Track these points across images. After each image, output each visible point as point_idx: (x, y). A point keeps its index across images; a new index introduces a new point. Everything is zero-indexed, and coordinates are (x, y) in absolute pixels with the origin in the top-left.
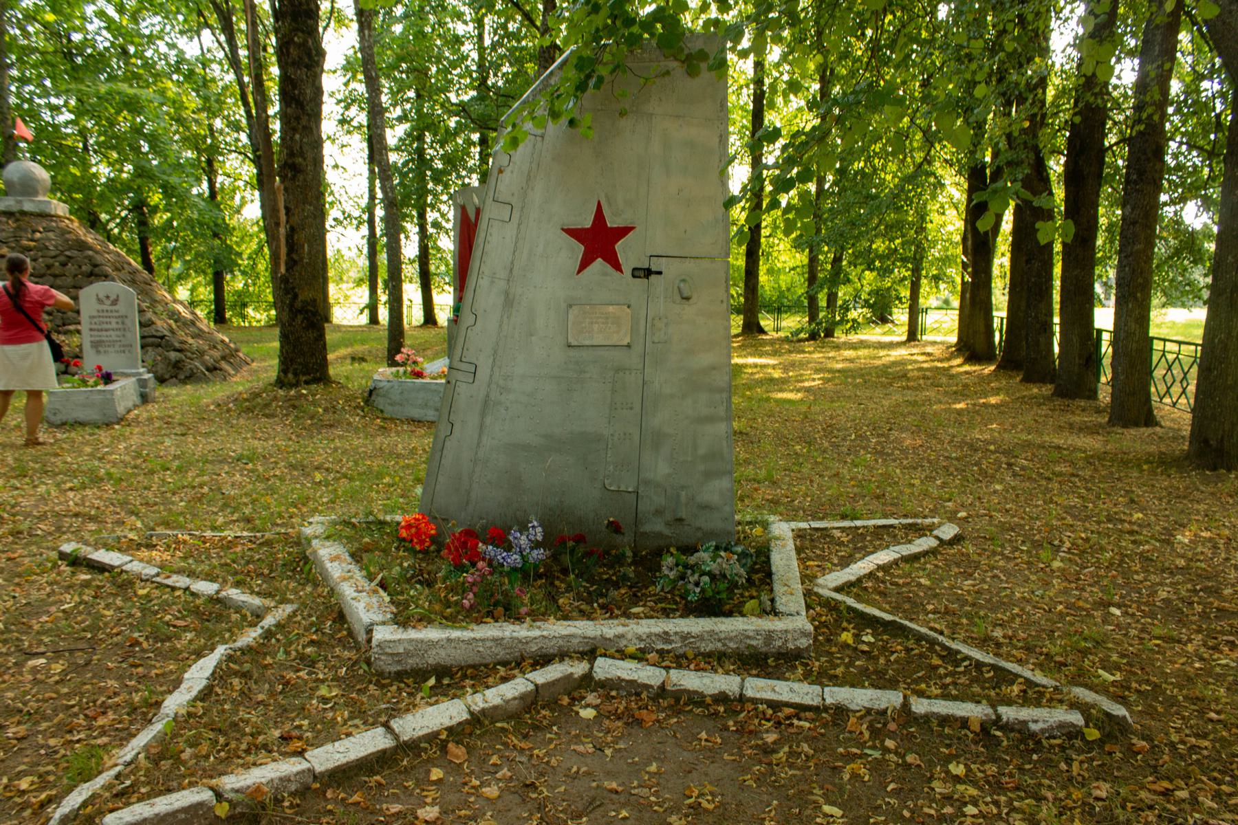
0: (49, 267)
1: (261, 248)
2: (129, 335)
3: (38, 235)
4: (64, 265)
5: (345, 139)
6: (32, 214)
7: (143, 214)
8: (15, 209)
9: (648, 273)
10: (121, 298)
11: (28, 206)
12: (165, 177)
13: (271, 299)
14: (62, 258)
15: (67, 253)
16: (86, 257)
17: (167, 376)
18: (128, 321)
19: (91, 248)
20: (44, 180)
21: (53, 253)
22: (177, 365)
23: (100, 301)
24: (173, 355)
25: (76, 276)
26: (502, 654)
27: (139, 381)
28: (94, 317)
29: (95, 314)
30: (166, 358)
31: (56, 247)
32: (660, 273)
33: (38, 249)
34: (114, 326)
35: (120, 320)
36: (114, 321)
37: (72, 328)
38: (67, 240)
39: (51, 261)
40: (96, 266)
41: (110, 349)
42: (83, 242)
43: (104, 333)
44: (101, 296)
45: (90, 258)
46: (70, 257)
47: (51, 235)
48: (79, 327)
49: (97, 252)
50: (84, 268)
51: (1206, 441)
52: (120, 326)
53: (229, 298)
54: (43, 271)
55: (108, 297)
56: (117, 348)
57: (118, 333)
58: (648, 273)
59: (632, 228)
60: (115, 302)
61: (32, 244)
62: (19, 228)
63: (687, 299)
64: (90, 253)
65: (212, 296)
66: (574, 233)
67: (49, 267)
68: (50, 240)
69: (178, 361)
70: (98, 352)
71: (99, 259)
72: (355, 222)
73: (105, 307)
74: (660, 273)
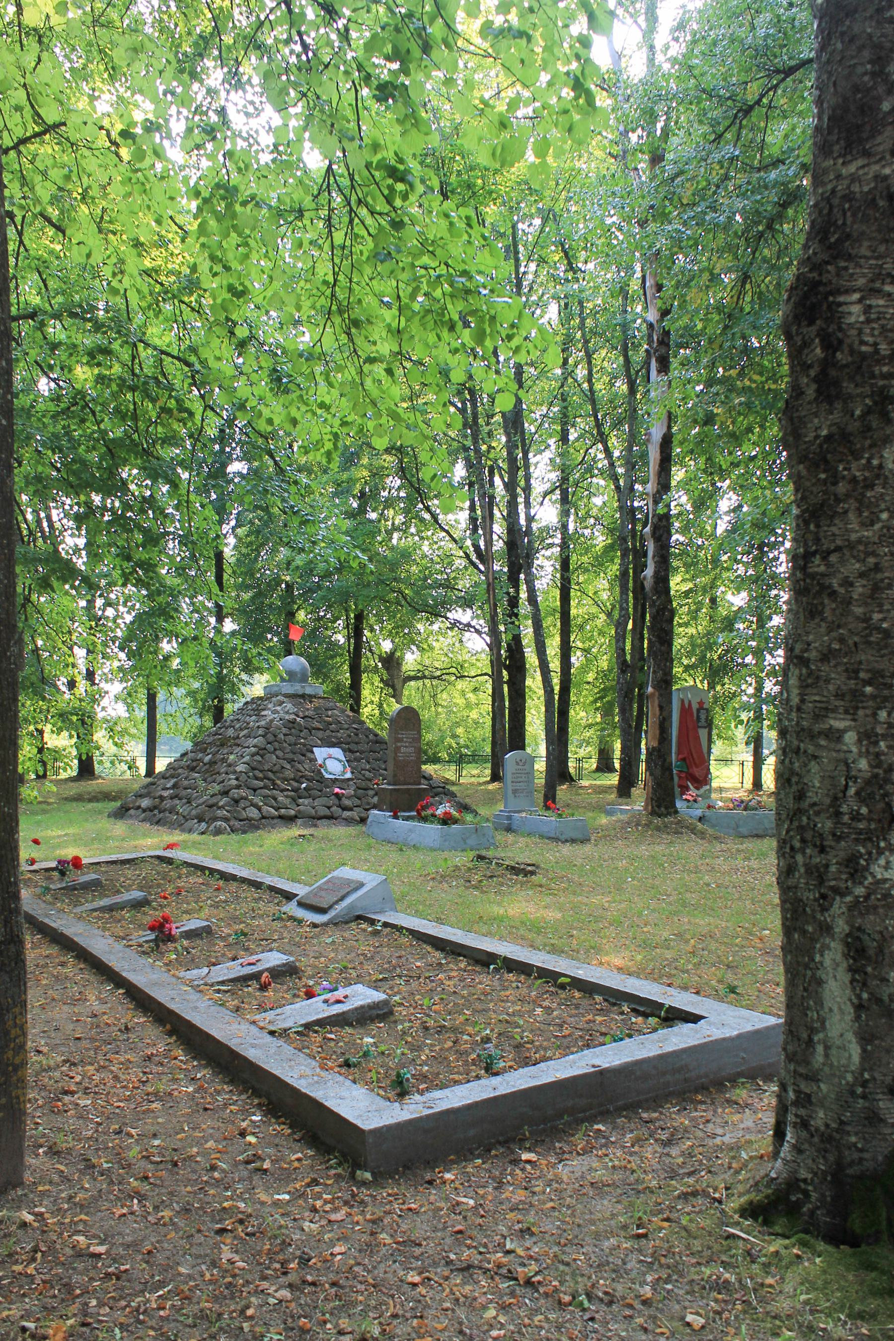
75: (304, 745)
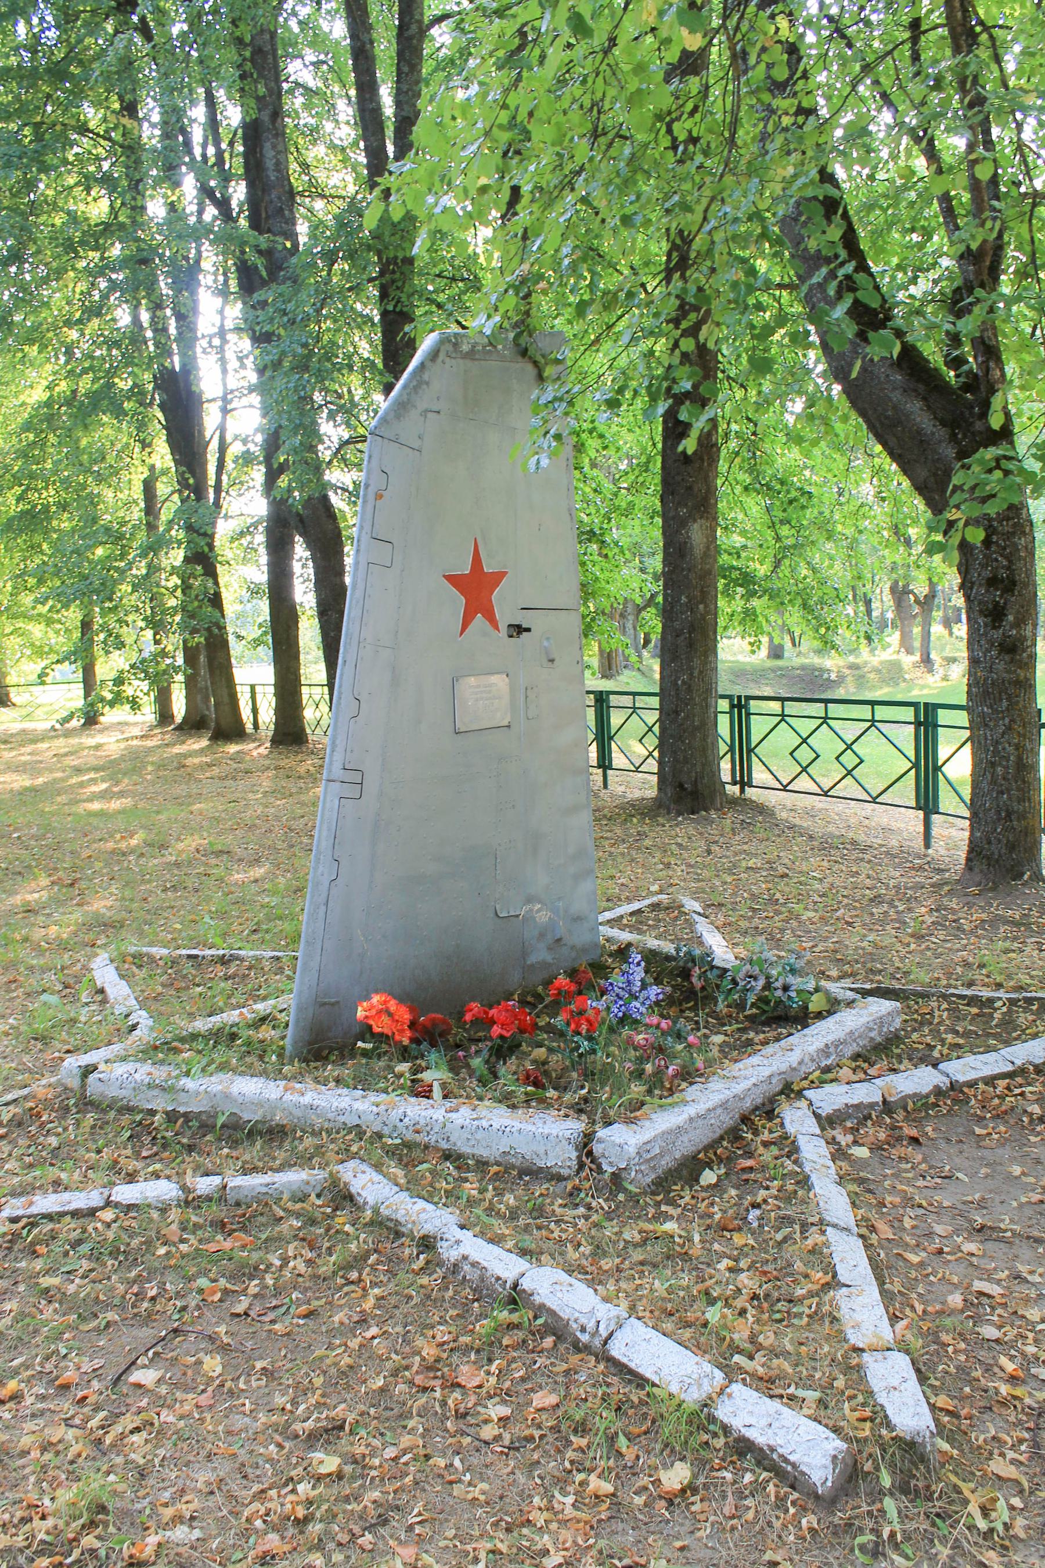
9: (518, 630)
26: (728, 1120)
32: (528, 630)
51: (681, 786)
58: (518, 630)
59: (503, 574)
63: (552, 661)
66: (451, 579)
74: (528, 630)
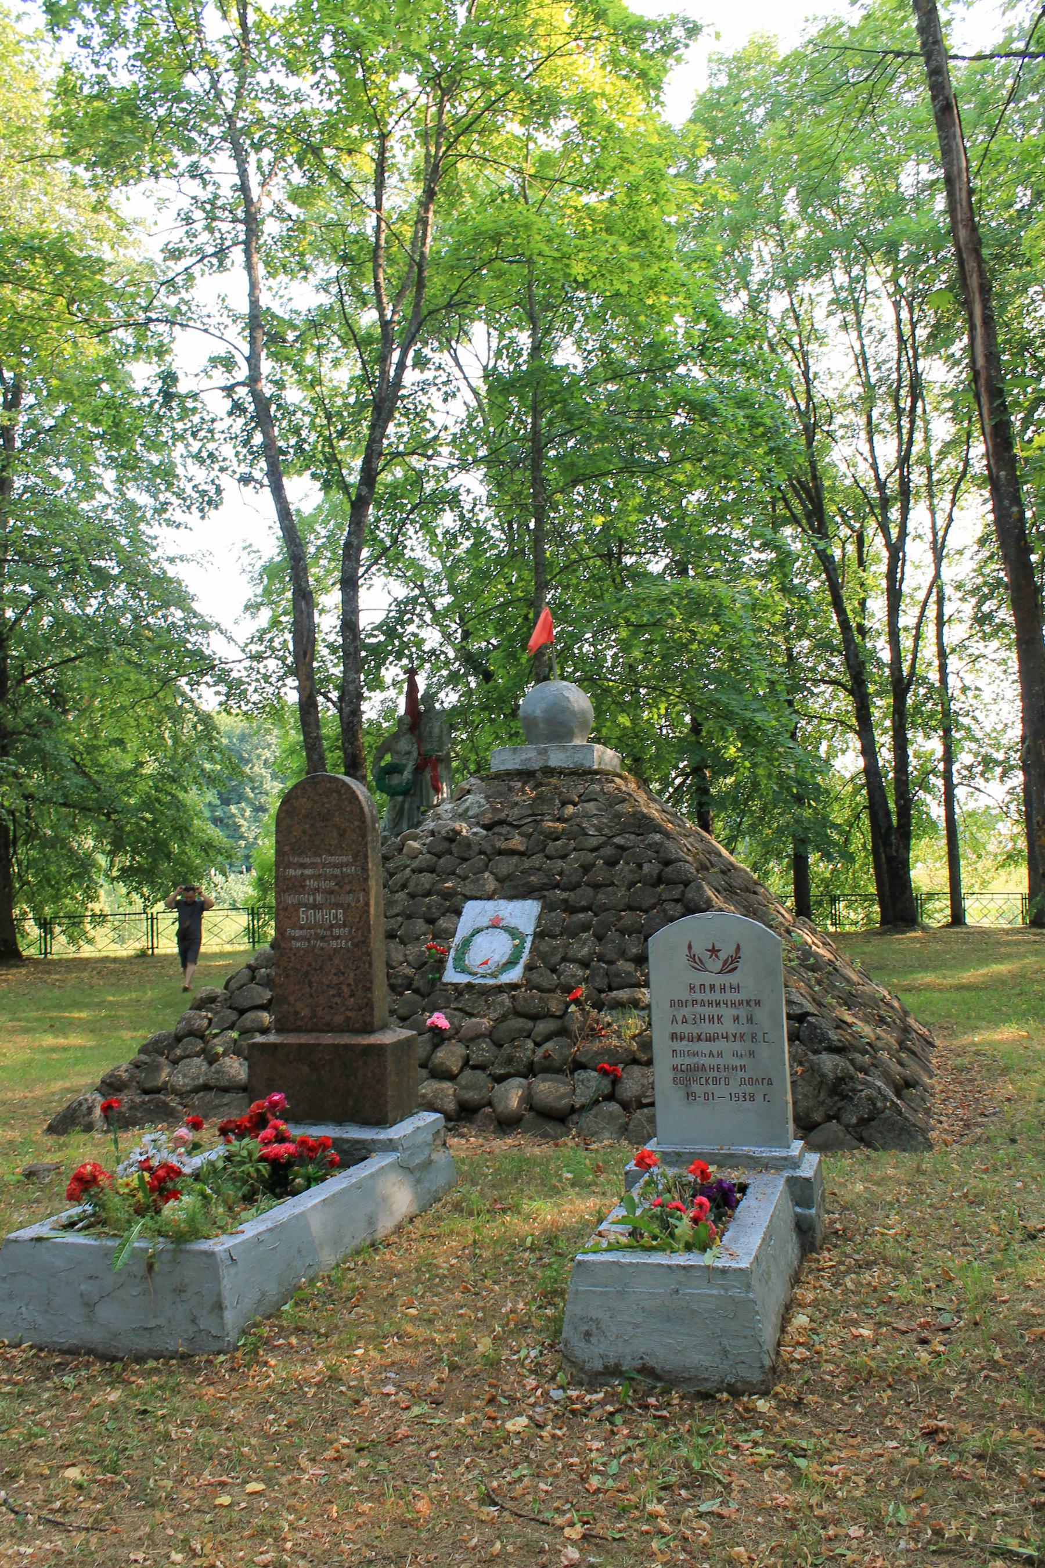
0: (586, 868)
1: (858, 817)
2: (763, 1051)
3: (570, 809)
4: (612, 863)
5: (977, 647)
6: (561, 772)
7: (704, 777)
8: (536, 766)
10: (744, 953)
11: (557, 759)
12: (748, 714)
13: (872, 889)
14: (608, 851)
15: (617, 840)
16: (650, 846)
17: (817, 1117)
18: (761, 1015)
19: (658, 829)
20: (583, 712)
21: (594, 842)
22: (839, 1089)
23: (696, 962)
24: (828, 1062)
25: (633, 884)
27: (793, 1183)
28: (682, 1003)
29: (685, 995)
30: (814, 1070)
31: (599, 829)
33: (571, 836)
34: (728, 1026)
35: (742, 1012)
36: (728, 1013)
37: (623, 995)
38: (618, 816)
39: (591, 856)
40: (667, 863)
41: (721, 1090)
42: (645, 816)
43: (705, 1047)
44: (699, 949)
45: (656, 848)
46: (622, 848)
47: (591, 807)
48: (678, 1061)
49: (667, 835)
50: (646, 868)
52: (744, 1028)
53: (815, 891)
54: (575, 879)
55: (714, 951)
56: (734, 1088)
57: (738, 1046)
60: (730, 966)
61: (560, 826)
62: (539, 797)
64: (657, 837)
65: (791, 888)
67: (586, 868)
68: (589, 817)
69: (841, 1080)
70: (690, 1095)
71: (673, 850)
72: (999, 770)
73: (707, 978)
75: (448, 895)
